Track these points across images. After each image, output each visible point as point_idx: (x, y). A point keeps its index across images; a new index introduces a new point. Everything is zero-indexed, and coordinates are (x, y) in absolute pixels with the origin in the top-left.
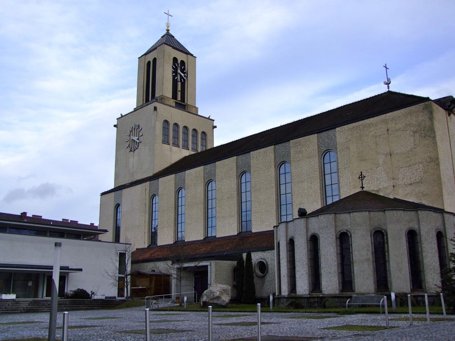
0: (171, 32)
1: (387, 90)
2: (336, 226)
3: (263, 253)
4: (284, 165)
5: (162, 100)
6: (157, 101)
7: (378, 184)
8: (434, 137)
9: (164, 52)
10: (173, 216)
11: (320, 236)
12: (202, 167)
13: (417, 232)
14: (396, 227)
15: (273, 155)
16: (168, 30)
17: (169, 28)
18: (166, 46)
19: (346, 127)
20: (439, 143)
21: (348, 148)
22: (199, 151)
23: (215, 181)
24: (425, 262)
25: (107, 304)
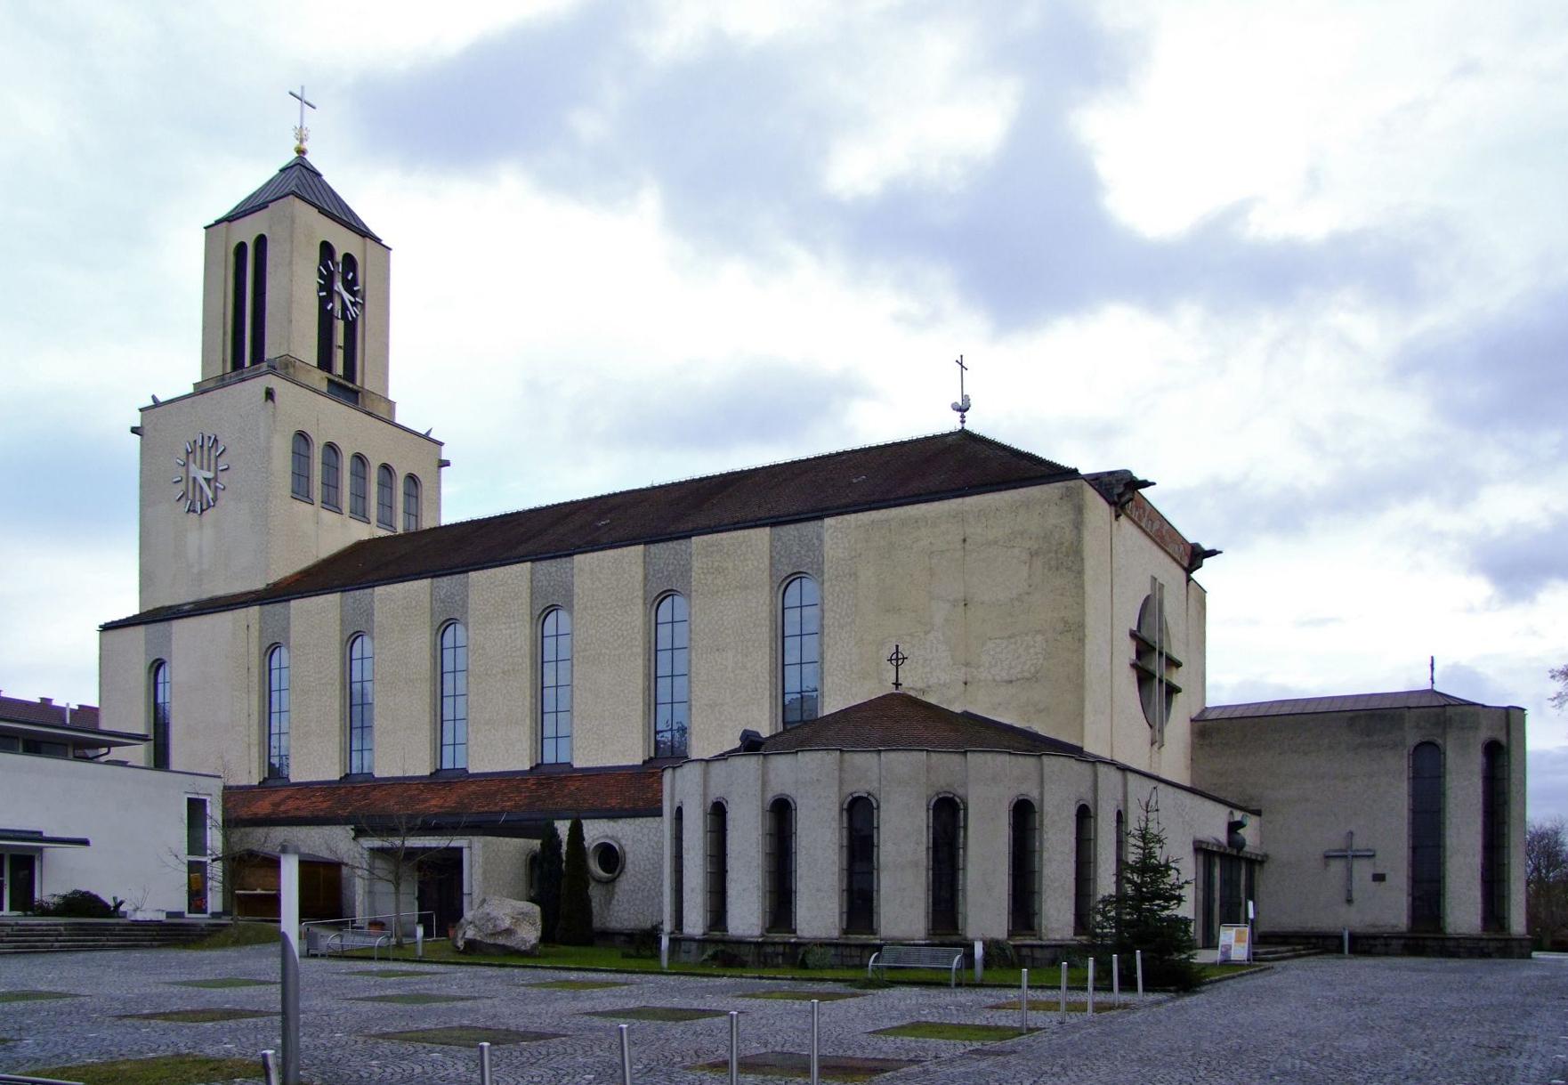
0: (312, 159)
1: (959, 427)
2: (841, 782)
3: (612, 823)
4: (669, 600)
5: (285, 368)
6: (273, 369)
7: (936, 679)
8: (1080, 573)
9: (293, 222)
10: (337, 706)
11: (799, 802)
12: (426, 582)
13: (1036, 804)
14: (989, 786)
15: (640, 571)
16: (301, 152)
17: (306, 145)
18: (298, 203)
19: (851, 518)
20: (1088, 588)
21: (854, 575)
22: (400, 531)
23: (466, 626)
24: (1045, 872)
25: (169, 934)
